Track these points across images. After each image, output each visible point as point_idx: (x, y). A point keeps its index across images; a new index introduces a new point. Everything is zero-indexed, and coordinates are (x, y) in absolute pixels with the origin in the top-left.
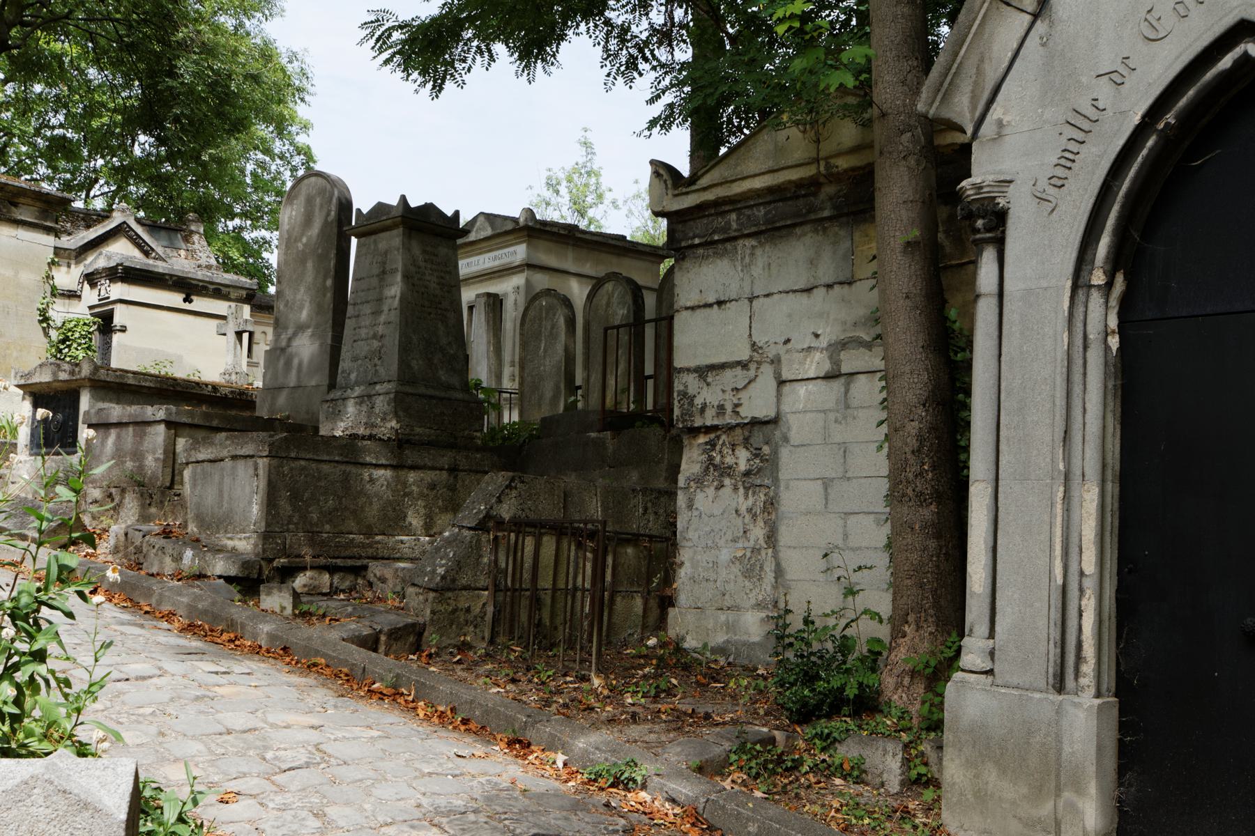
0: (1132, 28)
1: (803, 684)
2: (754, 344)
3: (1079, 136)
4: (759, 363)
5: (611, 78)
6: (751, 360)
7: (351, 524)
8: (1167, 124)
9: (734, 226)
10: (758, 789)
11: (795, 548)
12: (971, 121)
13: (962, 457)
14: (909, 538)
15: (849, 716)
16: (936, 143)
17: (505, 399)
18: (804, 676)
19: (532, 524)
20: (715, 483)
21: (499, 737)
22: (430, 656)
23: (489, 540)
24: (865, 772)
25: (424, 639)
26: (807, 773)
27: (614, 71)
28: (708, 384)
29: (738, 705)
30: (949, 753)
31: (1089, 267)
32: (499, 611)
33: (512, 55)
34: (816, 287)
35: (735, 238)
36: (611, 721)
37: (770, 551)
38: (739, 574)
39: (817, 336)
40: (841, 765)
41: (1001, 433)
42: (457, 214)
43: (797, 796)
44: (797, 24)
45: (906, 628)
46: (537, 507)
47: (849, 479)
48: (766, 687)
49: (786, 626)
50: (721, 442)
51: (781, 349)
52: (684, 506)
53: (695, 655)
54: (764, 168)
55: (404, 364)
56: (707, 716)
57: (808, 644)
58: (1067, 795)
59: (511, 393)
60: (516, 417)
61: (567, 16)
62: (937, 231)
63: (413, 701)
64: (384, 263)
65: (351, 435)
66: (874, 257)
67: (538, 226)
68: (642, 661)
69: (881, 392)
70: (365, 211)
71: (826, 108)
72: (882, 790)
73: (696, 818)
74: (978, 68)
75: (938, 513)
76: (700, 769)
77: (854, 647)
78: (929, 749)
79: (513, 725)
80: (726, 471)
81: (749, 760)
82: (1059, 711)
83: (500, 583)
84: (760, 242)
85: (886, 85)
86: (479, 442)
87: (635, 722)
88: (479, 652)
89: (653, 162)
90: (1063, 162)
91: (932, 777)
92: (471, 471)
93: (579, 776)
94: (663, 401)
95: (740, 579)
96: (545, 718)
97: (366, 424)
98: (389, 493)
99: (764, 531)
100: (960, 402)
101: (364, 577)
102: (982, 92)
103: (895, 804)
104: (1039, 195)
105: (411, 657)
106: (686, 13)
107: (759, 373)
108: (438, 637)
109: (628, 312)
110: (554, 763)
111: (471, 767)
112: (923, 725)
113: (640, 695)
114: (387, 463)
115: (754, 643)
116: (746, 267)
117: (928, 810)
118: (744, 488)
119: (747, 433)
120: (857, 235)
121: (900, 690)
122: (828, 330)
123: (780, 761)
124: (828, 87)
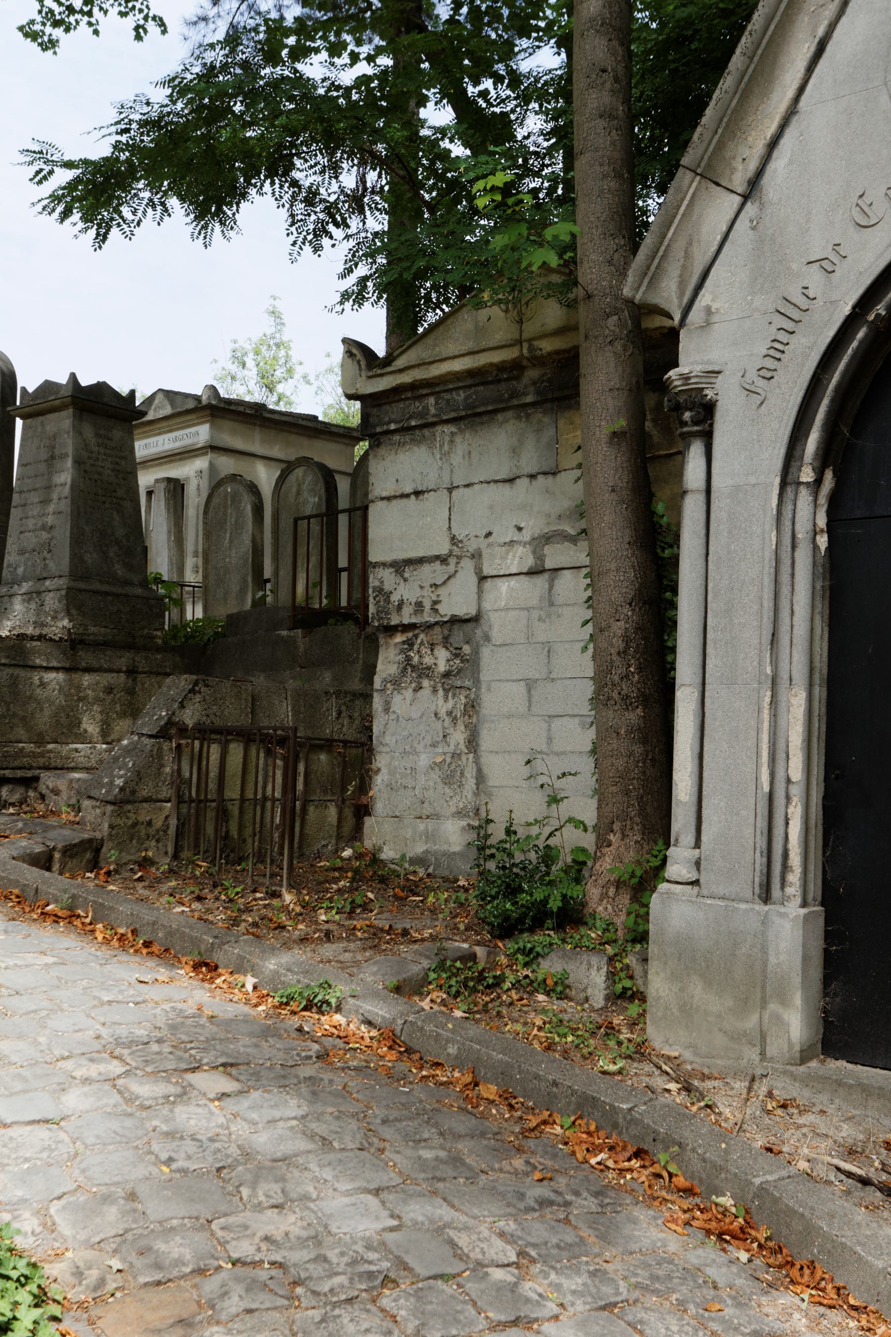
0: (843, 214)
1: (505, 896)
2: (453, 538)
3: (789, 326)
4: (459, 558)
5: (297, 248)
6: (450, 554)
7: (21, 732)
8: (878, 315)
9: (433, 411)
10: (458, 1008)
11: (497, 753)
12: (679, 307)
13: (669, 658)
14: (615, 744)
15: (553, 929)
16: (644, 325)
17: (188, 593)
18: (506, 888)
19: (219, 731)
20: (413, 685)
21: (184, 960)
22: (108, 873)
23: (171, 749)
24: (569, 987)
25: (102, 855)
26: (509, 990)
27: (300, 239)
28: (405, 580)
29: (437, 919)
30: (654, 967)
31: (798, 464)
32: (183, 824)
33: (188, 215)
34: (519, 477)
35: (434, 424)
36: (304, 940)
37: (471, 756)
38: (439, 780)
39: (520, 529)
40: (545, 980)
41: (708, 636)
42: (132, 393)
43: (499, 1014)
44: (498, 197)
45: (612, 837)
46: (222, 712)
47: (553, 680)
48: (466, 900)
49: (487, 836)
50: (419, 641)
51: (483, 543)
52: (380, 709)
53: (393, 866)
54: (464, 349)
55: (76, 558)
56: (405, 933)
57: (510, 855)
58: (772, 1007)
59: (194, 587)
60: (199, 614)
61: (251, 173)
62: (644, 420)
63: (91, 924)
64: (54, 447)
65: (18, 635)
66: (579, 448)
67: (222, 405)
68: (337, 874)
69: (586, 590)
70: (31, 389)
71: (530, 287)
72: (587, 1006)
73: (394, 1041)
74: (686, 252)
75: (644, 717)
76: (397, 990)
77: (558, 857)
78: (634, 961)
79: (199, 947)
80: (424, 672)
81: (449, 978)
82: (765, 921)
83: (184, 794)
84: (459, 429)
85: (592, 264)
86: (160, 641)
87: (329, 940)
88: (162, 869)
89: (345, 341)
90: (772, 352)
91: (638, 991)
92: (151, 673)
93: (270, 1000)
94: (357, 595)
95: (440, 785)
96: (233, 939)
97: (35, 623)
98: (62, 698)
99: (465, 735)
100: (667, 600)
101: (35, 789)
102: (690, 277)
103: (599, 1020)
104: (747, 387)
105: (88, 875)
106: (380, 176)
107: (459, 569)
108: (117, 853)
109: (320, 498)
110: (243, 986)
111: (153, 993)
112: (629, 937)
113: (334, 912)
114: (59, 665)
115: (454, 853)
116: (445, 455)
117: (633, 1025)
118: (444, 690)
119: (446, 632)
120: (561, 423)
121: (605, 901)
122: (531, 523)
123: (481, 978)
124: (530, 265)
